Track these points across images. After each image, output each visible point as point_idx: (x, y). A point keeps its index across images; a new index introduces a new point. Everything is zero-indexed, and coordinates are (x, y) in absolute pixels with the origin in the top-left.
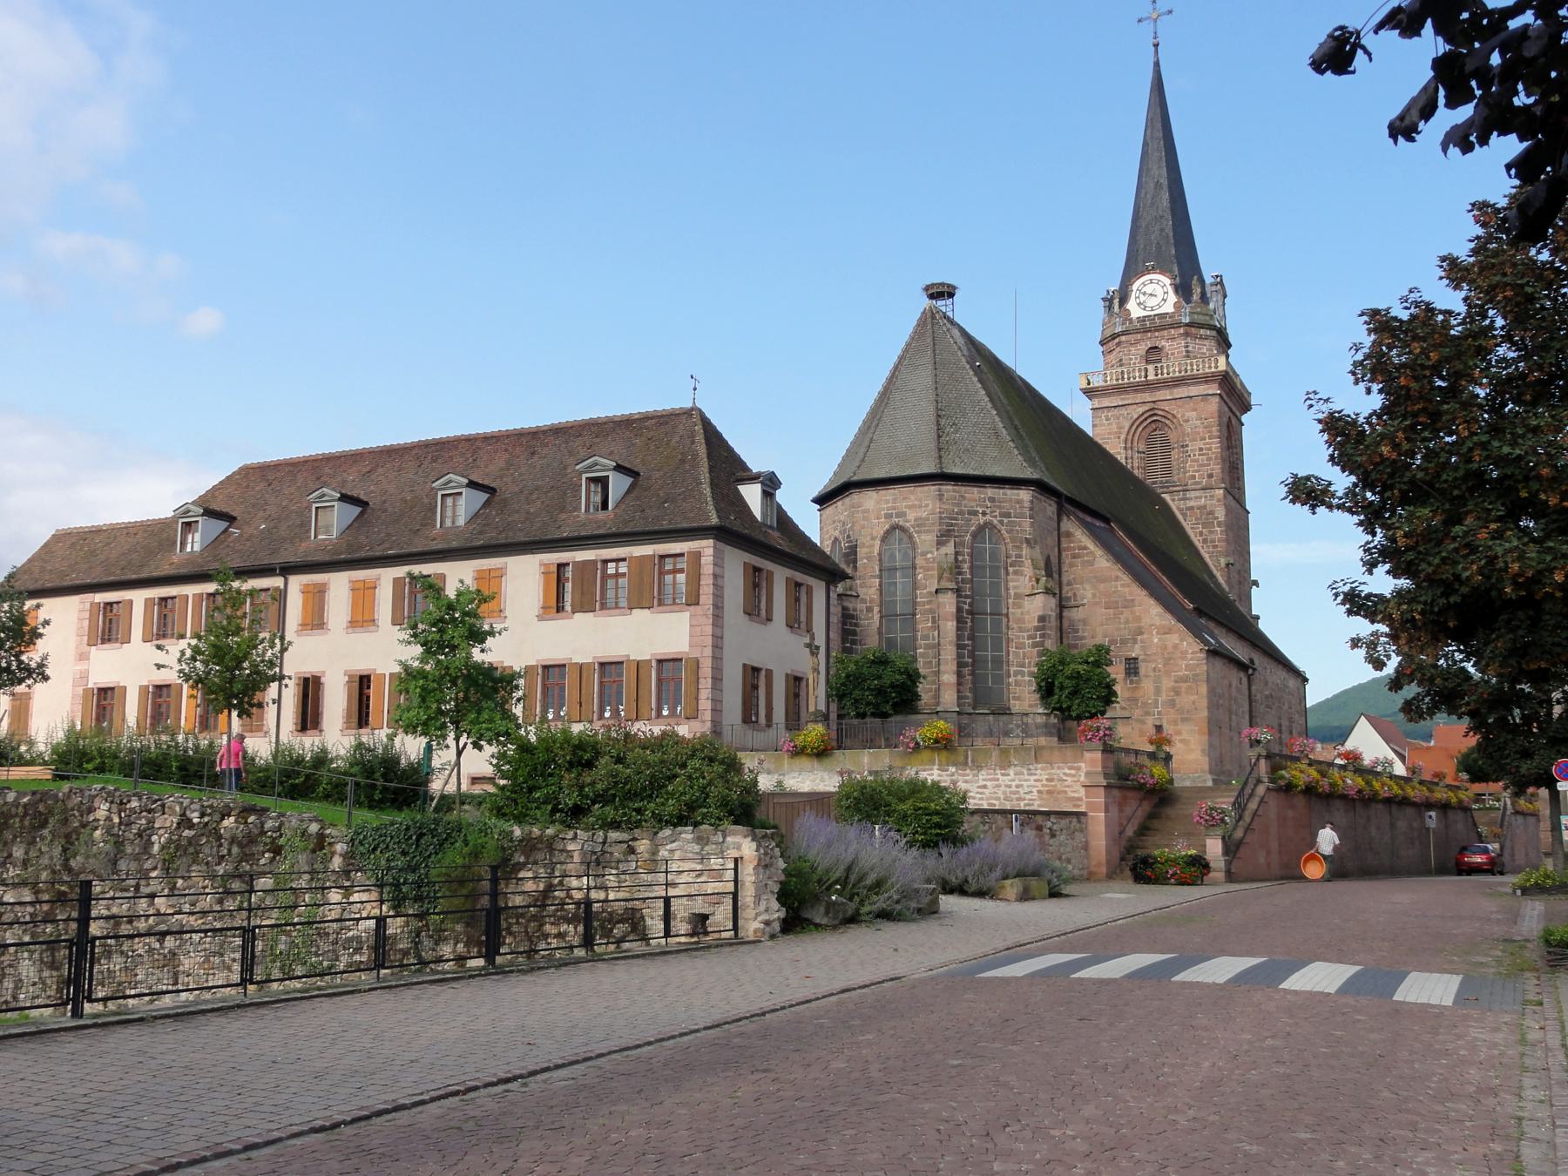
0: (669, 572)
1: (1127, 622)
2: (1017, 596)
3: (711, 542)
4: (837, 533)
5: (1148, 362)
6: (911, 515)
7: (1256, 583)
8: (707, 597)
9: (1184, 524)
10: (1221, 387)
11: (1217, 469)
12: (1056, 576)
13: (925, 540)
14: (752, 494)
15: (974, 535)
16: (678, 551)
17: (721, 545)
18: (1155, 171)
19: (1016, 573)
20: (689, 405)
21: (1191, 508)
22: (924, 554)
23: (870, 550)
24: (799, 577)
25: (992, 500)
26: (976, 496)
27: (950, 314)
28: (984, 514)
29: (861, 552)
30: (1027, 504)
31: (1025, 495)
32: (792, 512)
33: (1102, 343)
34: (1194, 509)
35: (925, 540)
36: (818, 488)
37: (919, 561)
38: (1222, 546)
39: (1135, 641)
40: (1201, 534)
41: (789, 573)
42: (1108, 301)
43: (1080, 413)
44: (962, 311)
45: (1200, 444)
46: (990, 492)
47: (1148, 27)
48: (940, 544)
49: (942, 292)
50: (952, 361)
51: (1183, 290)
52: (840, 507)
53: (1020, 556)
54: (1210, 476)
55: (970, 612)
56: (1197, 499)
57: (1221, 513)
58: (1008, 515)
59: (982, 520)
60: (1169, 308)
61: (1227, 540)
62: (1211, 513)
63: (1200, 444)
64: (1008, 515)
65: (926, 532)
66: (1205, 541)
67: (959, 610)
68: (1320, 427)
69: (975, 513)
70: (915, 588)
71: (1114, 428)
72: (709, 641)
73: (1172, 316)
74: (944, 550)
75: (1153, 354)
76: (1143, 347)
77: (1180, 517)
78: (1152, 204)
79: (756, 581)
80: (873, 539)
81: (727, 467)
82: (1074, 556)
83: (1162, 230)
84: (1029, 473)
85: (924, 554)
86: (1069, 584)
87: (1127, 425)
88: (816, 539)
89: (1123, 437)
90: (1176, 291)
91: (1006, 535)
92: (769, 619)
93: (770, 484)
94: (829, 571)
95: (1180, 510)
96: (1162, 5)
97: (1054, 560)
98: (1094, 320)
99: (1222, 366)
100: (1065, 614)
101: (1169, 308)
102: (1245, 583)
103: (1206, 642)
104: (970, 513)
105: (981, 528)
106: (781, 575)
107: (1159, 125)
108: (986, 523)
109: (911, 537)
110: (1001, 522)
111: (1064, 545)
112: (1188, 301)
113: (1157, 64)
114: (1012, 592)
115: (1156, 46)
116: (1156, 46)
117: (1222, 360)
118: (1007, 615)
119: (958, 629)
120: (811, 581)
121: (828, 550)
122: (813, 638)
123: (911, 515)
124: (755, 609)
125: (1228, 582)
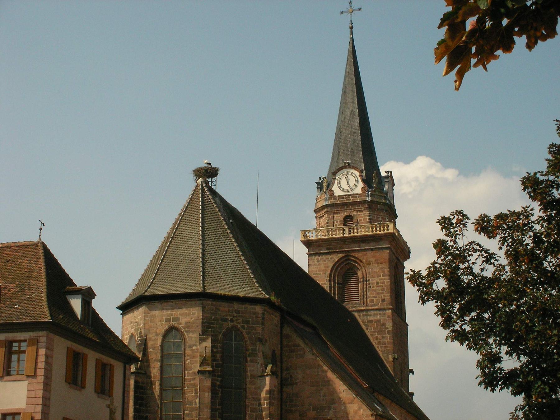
0: (15, 352)
1: (325, 395)
2: (253, 376)
3: (44, 333)
4: (133, 330)
5: (345, 225)
6: (183, 320)
7: (412, 371)
8: (41, 372)
9: (366, 332)
10: (390, 243)
11: (387, 296)
12: (279, 364)
13: (192, 337)
14: (76, 304)
15: (224, 335)
16: (22, 338)
17: (51, 335)
18: (349, 100)
19: (252, 361)
20: (36, 240)
21: (371, 321)
22: (191, 347)
23: (155, 342)
24: (106, 359)
25: (237, 312)
26: (227, 309)
27: (214, 188)
28: (232, 321)
29: (150, 344)
30: (260, 315)
31: (258, 309)
32: (103, 314)
33: (316, 211)
34: (372, 320)
35: (192, 337)
36: (122, 298)
37: (188, 352)
38: (390, 346)
39: (330, 408)
40: (377, 338)
41: (98, 355)
42: (320, 185)
43: (300, 256)
44: (223, 186)
45: (377, 279)
46: (236, 306)
47: (347, 16)
48: (202, 340)
49: (208, 173)
50: (215, 216)
51: (367, 181)
52: (138, 314)
53: (255, 350)
54: (383, 300)
55: (220, 387)
56: (374, 317)
57: (389, 325)
58: (248, 322)
59: (230, 324)
60: (358, 190)
61: (394, 344)
62: (384, 324)
63: (377, 279)
64: (248, 322)
65: (193, 332)
66: (379, 343)
67: (213, 385)
68: (483, 386)
69: (226, 320)
70: (185, 369)
71: (322, 267)
72: (40, 401)
73: (360, 195)
74: (204, 344)
75: (348, 219)
76: (341, 216)
77: (364, 327)
78: (349, 125)
79: (76, 362)
80: (157, 335)
81: (59, 282)
82: (291, 351)
83: (354, 141)
84: (263, 295)
85: (191, 347)
86: (287, 369)
87: (331, 265)
88: (118, 333)
89: (328, 273)
90: (364, 181)
91: (246, 336)
92: (83, 387)
93: (88, 295)
94: (123, 354)
95: (363, 322)
96: (355, 5)
97: (278, 353)
98: (312, 198)
99: (391, 230)
100: (285, 389)
101: (358, 190)
102: (404, 370)
103: (375, 410)
104: (223, 320)
105: (229, 331)
106: (92, 357)
107: (353, 76)
108: (232, 327)
109: (182, 334)
110: (243, 327)
111: (285, 343)
112: (370, 187)
113: (352, 39)
114: (249, 374)
115: (352, 28)
116: (352, 28)
117: (391, 226)
118: (246, 389)
119: (212, 398)
120: (113, 362)
121: (126, 342)
122: (112, 402)
123: (183, 320)
124: (75, 378)
125: (394, 371)
